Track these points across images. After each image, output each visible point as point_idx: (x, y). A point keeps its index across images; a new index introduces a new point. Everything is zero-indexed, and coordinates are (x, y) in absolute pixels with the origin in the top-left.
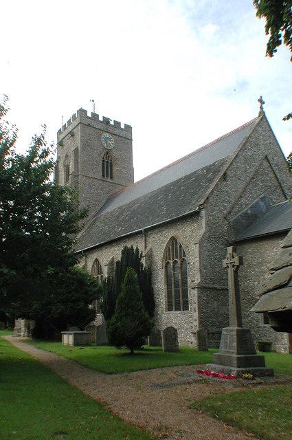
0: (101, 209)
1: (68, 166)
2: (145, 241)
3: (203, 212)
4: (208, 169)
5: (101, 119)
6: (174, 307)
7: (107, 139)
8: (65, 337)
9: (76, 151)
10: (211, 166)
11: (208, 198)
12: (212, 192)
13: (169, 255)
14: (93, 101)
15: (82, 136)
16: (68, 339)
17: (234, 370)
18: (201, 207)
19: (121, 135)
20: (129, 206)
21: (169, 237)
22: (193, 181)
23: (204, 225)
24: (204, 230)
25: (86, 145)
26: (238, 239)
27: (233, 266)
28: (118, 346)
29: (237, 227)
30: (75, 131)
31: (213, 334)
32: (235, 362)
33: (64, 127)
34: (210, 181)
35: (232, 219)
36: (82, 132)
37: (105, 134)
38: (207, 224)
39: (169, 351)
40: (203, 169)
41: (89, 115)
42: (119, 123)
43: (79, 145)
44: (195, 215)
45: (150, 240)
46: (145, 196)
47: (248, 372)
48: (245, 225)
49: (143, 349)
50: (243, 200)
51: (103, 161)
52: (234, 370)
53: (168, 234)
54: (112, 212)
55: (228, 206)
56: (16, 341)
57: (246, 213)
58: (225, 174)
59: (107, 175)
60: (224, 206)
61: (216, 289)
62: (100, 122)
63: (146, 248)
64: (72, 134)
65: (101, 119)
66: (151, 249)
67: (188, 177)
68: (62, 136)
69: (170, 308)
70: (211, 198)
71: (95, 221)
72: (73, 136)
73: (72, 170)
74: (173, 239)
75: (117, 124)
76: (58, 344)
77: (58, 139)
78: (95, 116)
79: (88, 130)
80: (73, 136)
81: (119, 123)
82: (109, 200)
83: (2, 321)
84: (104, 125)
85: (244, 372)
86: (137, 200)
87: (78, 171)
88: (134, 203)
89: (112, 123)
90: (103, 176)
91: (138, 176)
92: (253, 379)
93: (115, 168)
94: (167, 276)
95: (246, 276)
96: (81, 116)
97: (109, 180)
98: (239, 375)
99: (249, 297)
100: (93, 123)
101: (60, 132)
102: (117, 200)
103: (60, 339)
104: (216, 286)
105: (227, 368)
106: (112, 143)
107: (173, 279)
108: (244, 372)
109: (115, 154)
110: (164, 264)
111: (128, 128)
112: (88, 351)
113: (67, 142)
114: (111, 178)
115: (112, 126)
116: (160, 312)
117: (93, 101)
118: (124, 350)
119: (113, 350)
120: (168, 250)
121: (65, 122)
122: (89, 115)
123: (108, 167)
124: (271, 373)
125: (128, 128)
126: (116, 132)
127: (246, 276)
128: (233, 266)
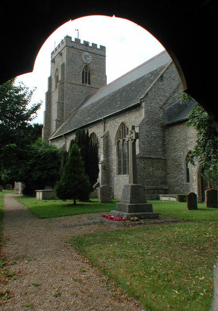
0: (80, 106)
1: (58, 76)
2: (104, 126)
3: (143, 104)
4: (152, 73)
5: (82, 42)
6: (122, 172)
7: (86, 56)
8: (38, 193)
9: (63, 65)
10: (154, 71)
11: (147, 94)
12: (151, 90)
13: (120, 135)
14: (77, 30)
15: (67, 55)
16: (39, 194)
17: (125, 214)
18: (142, 100)
19: (97, 53)
20: (98, 102)
21: (120, 123)
22: (141, 82)
23: (143, 113)
24: (143, 116)
25: (70, 60)
26: (170, 122)
27: (132, 140)
28: (63, 197)
29: (170, 114)
30: (63, 51)
31: (148, 190)
32: (127, 209)
33: (56, 49)
34: (151, 82)
35: (167, 108)
36: (67, 53)
37: (85, 53)
38: (146, 112)
39: (104, 202)
40: (149, 74)
41: (73, 40)
42: (96, 45)
43: (65, 61)
44: (137, 107)
45: (108, 125)
46: (109, 95)
47: (135, 216)
48: (177, 112)
49: (90, 201)
50: (176, 95)
51: (83, 72)
52: (125, 214)
53: (119, 121)
54: (86, 107)
55: (164, 99)
56: (11, 199)
57: (178, 104)
58: (162, 76)
59: (86, 81)
60: (161, 100)
61: (152, 158)
62: (82, 44)
63: (104, 130)
64: (60, 54)
65: (82, 42)
66: (108, 132)
67: (138, 80)
68: (54, 55)
69: (119, 173)
70: (150, 94)
71: (74, 114)
72: (61, 55)
73: (60, 78)
74: (123, 124)
75: (94, 45)
76: (33, 199)
77: (52, 57)
78: (78, 41)
79: (72, 51)
80: (61, 55)
81: (96, 45)
82: (86, 99)
83: (7, 184)
84: (84, 47)
85: (132, 216)
86: (103, 98)
87: (64, 79)
88: (101, 100)
89: (90, 45)
90: (83, 82)
91: (109, 81)
92: (137, 220)
93: (92, 77)
94: (118, 150)
95: (175, 149)
96: (67, 41)
97: (87, 85)
98: (128, 218)
99: (177, 164)
100: (76, 46)
101: (53, 53)
102: (91, 99)
103: (35, 196)
104: (153, 156)
105: (122, 213)
106: (90, 59)
107: (122, 152)
108: (132, 216)
109: (92, 66)
110: (117, 142)
111: (103, 48)
112: (50, 202)
113: (57, 60)
114: (89, 84)
115: (90, 47)
116: (113, 176)
117: (77, 30)
118: (69, 202)
119: (60, 202)
120: (119, 132)
121: (56, 46)
122: (73, 40)
123: (86, 77)
124: (156, 216)
125: (103, 48)
126: (94, 51)
127: (175, 149)
128: (132, 140)
